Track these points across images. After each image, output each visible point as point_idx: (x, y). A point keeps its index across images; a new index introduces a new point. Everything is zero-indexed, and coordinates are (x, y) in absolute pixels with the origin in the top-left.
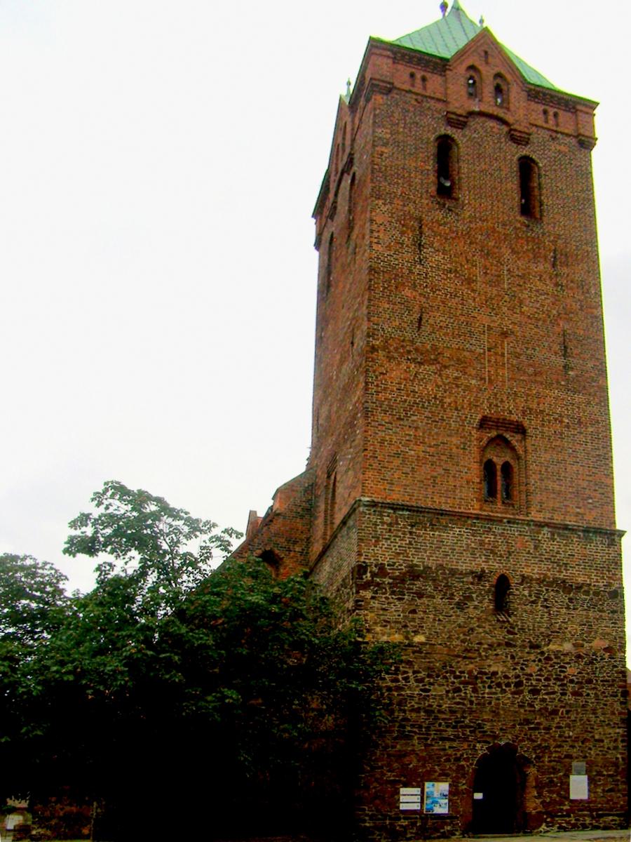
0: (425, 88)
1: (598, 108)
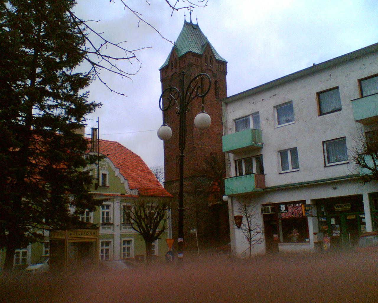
0: (198, 63)
1: (228, 63)
